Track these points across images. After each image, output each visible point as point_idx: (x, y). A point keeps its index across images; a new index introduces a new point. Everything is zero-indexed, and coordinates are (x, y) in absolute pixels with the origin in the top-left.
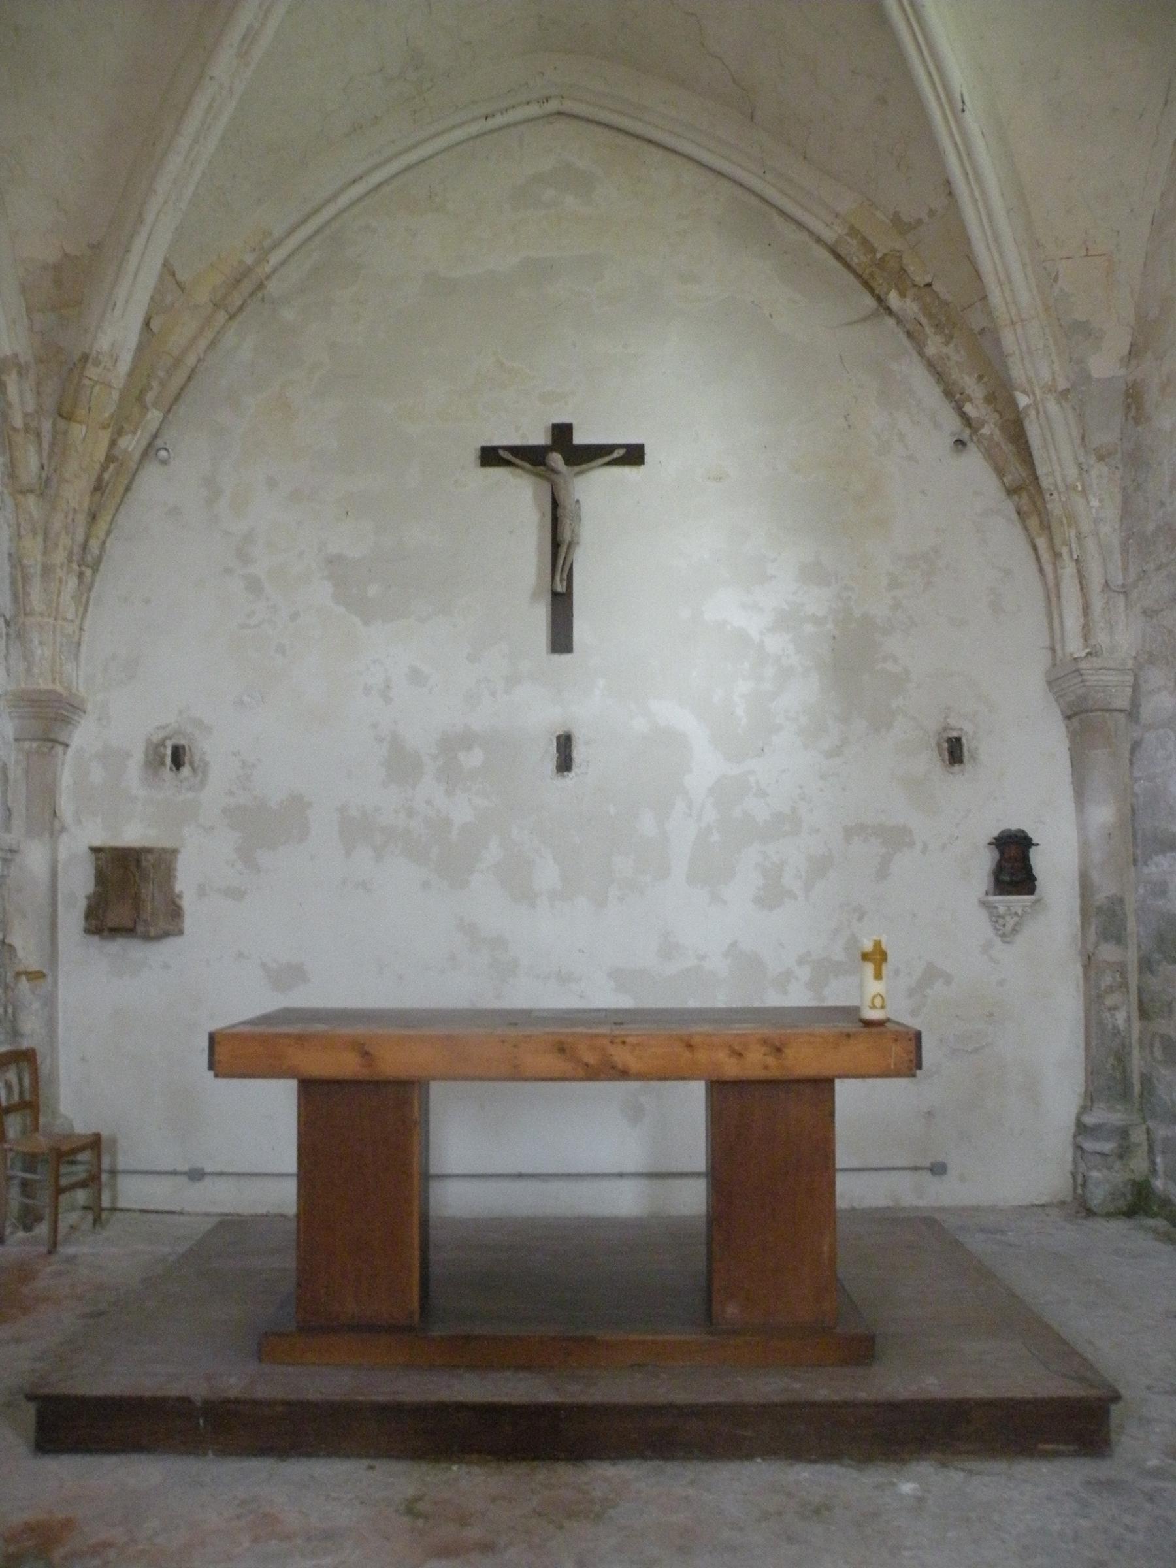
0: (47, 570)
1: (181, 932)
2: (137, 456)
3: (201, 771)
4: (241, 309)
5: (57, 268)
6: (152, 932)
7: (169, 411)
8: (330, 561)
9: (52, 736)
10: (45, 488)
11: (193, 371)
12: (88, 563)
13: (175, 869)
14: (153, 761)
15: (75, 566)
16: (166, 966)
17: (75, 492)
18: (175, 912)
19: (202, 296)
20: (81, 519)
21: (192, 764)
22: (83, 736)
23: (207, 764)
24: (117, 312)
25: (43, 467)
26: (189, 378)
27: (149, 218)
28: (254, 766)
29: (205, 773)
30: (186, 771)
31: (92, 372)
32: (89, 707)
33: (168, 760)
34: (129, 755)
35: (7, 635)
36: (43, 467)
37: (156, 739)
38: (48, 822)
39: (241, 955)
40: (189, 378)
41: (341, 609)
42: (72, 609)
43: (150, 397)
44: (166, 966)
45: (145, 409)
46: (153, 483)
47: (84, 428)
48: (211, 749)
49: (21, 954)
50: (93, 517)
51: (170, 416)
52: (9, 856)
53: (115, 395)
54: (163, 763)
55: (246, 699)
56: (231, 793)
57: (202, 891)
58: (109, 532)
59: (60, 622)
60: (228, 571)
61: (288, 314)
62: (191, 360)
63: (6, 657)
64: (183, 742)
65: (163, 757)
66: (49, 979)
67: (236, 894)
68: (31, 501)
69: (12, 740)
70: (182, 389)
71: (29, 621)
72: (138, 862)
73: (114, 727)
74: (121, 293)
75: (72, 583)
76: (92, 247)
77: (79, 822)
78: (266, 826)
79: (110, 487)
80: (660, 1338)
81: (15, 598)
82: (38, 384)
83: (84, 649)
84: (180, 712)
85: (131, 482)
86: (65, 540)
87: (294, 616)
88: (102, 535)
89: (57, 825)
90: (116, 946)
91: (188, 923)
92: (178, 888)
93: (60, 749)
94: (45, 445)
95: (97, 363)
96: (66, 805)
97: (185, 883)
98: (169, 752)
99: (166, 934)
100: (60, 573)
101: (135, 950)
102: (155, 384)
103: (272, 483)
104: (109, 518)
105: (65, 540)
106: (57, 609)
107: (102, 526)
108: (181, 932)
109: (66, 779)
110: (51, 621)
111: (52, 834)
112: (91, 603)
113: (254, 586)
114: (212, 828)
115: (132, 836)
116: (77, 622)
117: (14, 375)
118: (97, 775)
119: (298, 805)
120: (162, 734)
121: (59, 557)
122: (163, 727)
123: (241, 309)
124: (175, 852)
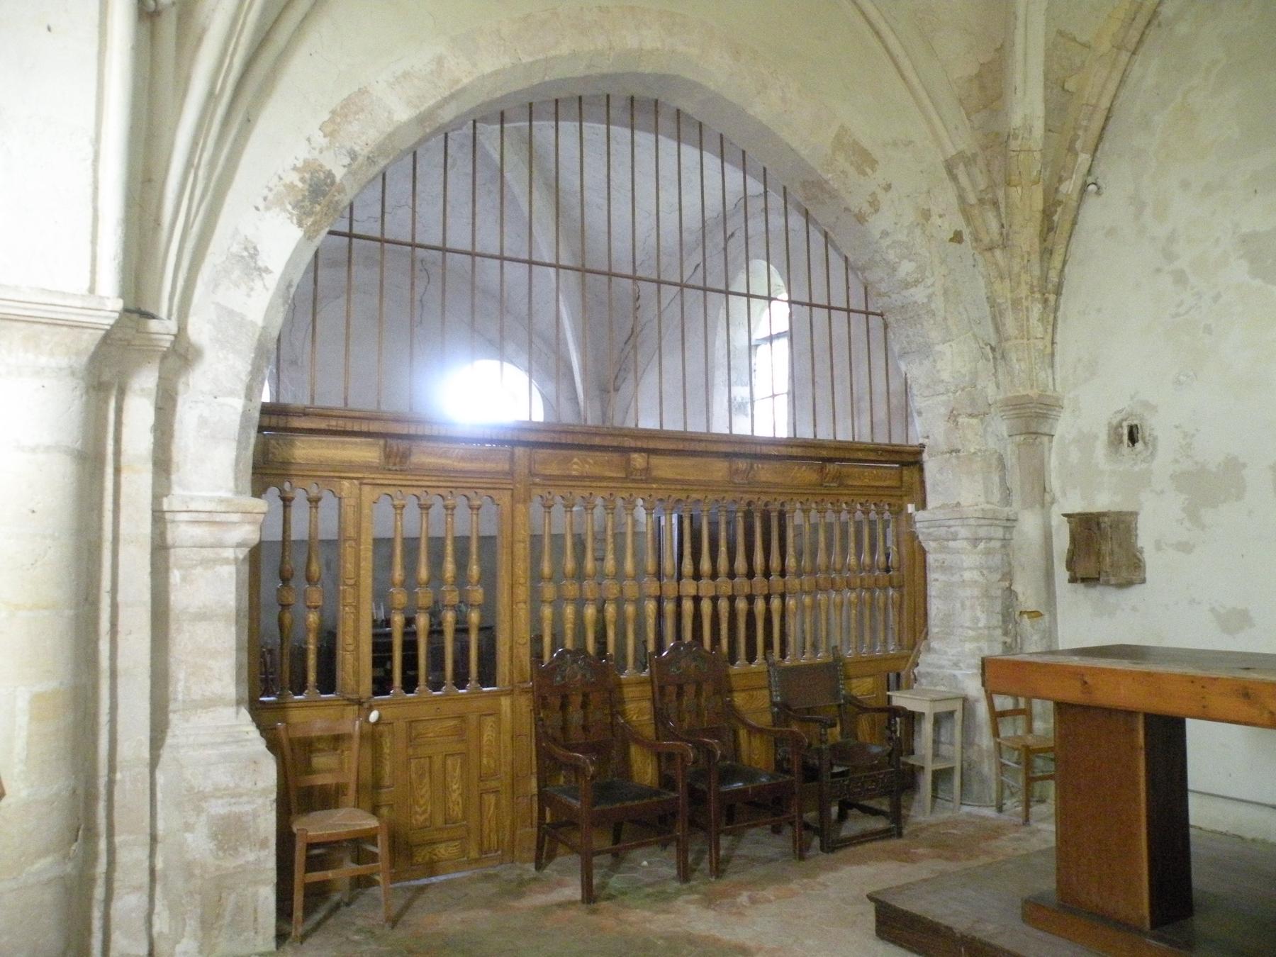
0: (1016, 303)
1: (1143, 581)
2: (1075, 196)
3: (1152, 444)
4: (1140, 42)
5: (979, 76)
6: (1113, 581)
7: (1096, 150)
8: (1244, 240)
9: (1033, 430)
10: (1005, 243)
11: (1109, 110)
12: (1051, 292)
13: (1136, 529)
14: (1115, 441)
15: (1037, 295)
16: (1134, 609)
17: (1027, 237)
18: (1136, 564)
19: (1105, 46)
20: (1035, 258)
21: (1143, 439)
22: (1064, 427)
23: (1155, 439)
24: (1019, 94)
25: (1002, 226)
26: (1107, 119)
27: (1021, 12)
28: (1193, 435)
29: (1154, 447)
30: (1139, 445)
31: (1014, 144)
32: (1066, 402)
33: (1126, 438)
34: (1096, 437)
35: (994, 358)
36: (1002, 226)
37: (1115, 422)
38: (1041, 495)
39: (1192, 601)
40: (1107, 119)
41: (1258, 283)
42: (1041, 329)
43: (1078, 145)
44: (1134, 609)
45: (1077, 154)
46: (1094, 215)
47: (1019, 189)
48: (1158, 426)
49: (1021, 597)
50: (1047, 253)
51: (1098, 154)
52: (1008, 524)
53: (1038, 155)
54: (1121, 442)
55: (1182, 378)
56: (1176, 461)
57: (1158, 546)
58: (1064, 263)
59: (1032, 341)
60: (1158, 270)
61: (1182, 29)
62: (1105, 103)
63: (995, 375)
64: (1135, 422)
65: (1122, 435)
66: (1047, 617)
67: (1185, 547)
68: (998, 253)
69: (1005, 434)
70: (1103, 129)
71: (1007, 345)
72: (1098, 524)
73: (1084, 417)
74: (1018, 79)
75: (1037, 309)
76: (997, 50)
77: (1064, 494)
78: (1209, 486)
79: (1055, 225)
80: (287, 675)
81: (997, 330)
82: (988, 165)
83: (1057, 358)
84: (1132, 398)
85: (1076, 217)
86: (1024, 277)
87: (1216, 298)
88: (1059, 266)
89: (1048, 497)
90: (1095, 592)
91: (1149, 574)
92: (1140, 544)
93: (1046, 439)
94: (1003, 210)
95: (1016, 138)
96: (1055, 483)
97: (1145, 539)
98: (1126, 431)
99: (1129, 584)
100: (1025, 303)
101: (1113, 596)
102: (1080, 133)
103: (1185, 185)
104: (1063, 250)
105: (1024, 277)
106: (1028, 332)
107: (1057, 261)
108: (1143, 581)
109: (1053, 462)
110: (1025, 341)
111: (1043, 506)
112: (1060, 321)
113: (1180, 278)
114: (1162, 492)
115: (1102, 502)
116: (1049, 338)
117: (961, 167)
118: (1074, 456)
119: (1233, 466)
120: (1119, 417)
121: (1024, 291)
122: (1120, 412)
123: (1140, 42)
124: (1134, 514)
